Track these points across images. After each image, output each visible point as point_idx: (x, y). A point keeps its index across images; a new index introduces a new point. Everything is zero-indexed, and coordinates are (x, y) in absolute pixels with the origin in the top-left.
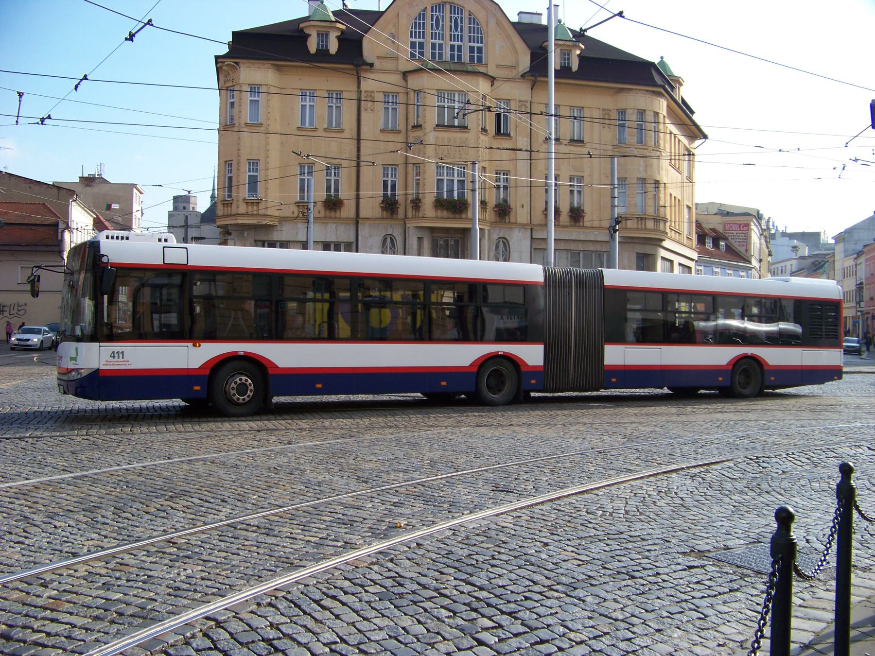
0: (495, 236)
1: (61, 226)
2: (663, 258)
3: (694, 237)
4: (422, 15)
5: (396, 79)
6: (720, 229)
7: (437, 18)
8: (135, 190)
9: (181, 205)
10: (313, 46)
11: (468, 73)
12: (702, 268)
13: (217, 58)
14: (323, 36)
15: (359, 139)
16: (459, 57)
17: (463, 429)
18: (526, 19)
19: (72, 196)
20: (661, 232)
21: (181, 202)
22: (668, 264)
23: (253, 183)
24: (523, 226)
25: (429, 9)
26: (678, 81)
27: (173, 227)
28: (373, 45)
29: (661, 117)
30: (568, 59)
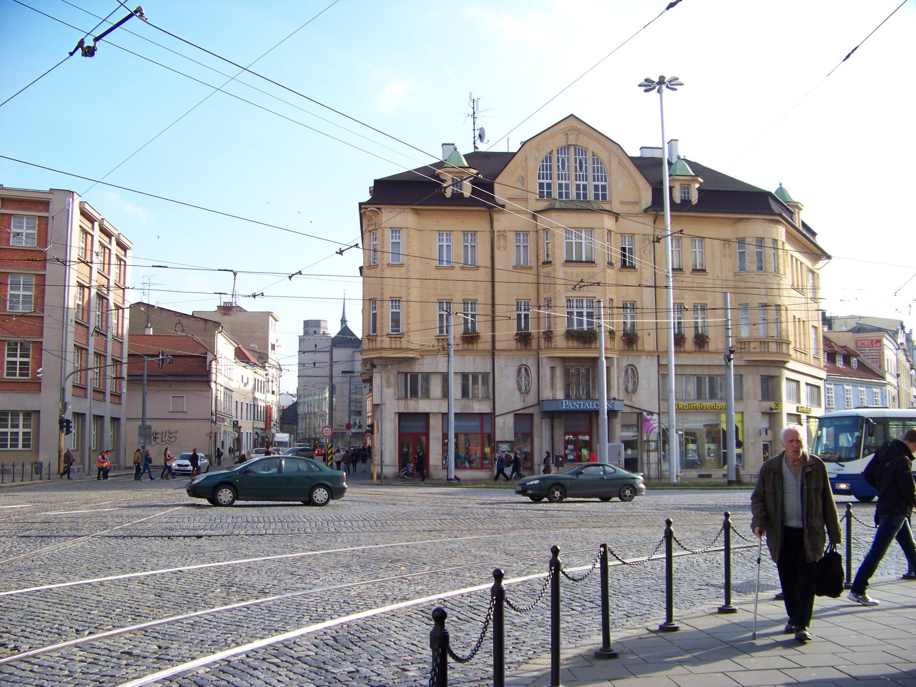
0: (624, 364)
1: (210, 357)
2: (788, 379)
3: (823, 357)
4: (548, 159)
6: (852, 346)
8: (271, 318)
9: (312, 330)
11: (592, 211)
12: (832, 386)
13: (361, 204)
14: (457, 183)
15: (493, 282)
16: (585, 196)
17: (583, 529)
18: (648, 154)
19: (218, 327)
20: (785, 354)
21: (312, 327)
22: (794, 384)
23: (396, 320)
24: (650, 353)
25: (555, 152)
26: (797, 206)
27: (304, 352)
29: (780, 243)
30: (688, 193)
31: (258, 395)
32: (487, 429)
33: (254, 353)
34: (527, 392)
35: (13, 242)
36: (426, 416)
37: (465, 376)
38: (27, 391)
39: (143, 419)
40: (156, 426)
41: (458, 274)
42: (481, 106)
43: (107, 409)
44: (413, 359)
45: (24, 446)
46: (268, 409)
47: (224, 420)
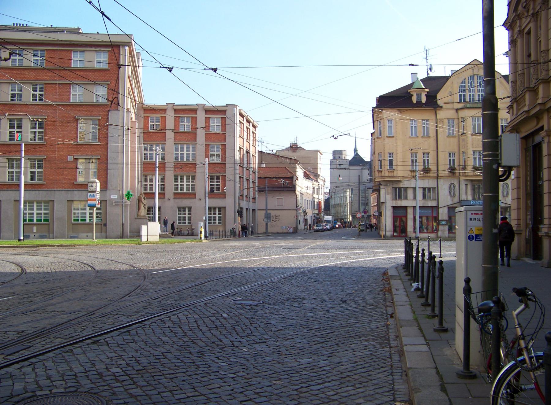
4: (464, 82)
5: (455, 111)
7: (471, 82)
9: (337, 156)
10: (414, 100)
14: (419, 95)
21: (337, 154)
23: (391, 162)
25: (467, 78)
28: (442, 97)
31: (315, 196)
32: (435, 215)
33: (312, 174)
34: (454, 196)
35: (73, 65)
36: (406, 208)
37: (424, 189)
38: (220, 198)
39: (266, 209)
40: (273, 213)
41: (420, 140)
42: (430, 53)
43: (251, 206)
44: (400, 181)
45: (219, 223)
46: (320, 203)
47: (300, 210)
